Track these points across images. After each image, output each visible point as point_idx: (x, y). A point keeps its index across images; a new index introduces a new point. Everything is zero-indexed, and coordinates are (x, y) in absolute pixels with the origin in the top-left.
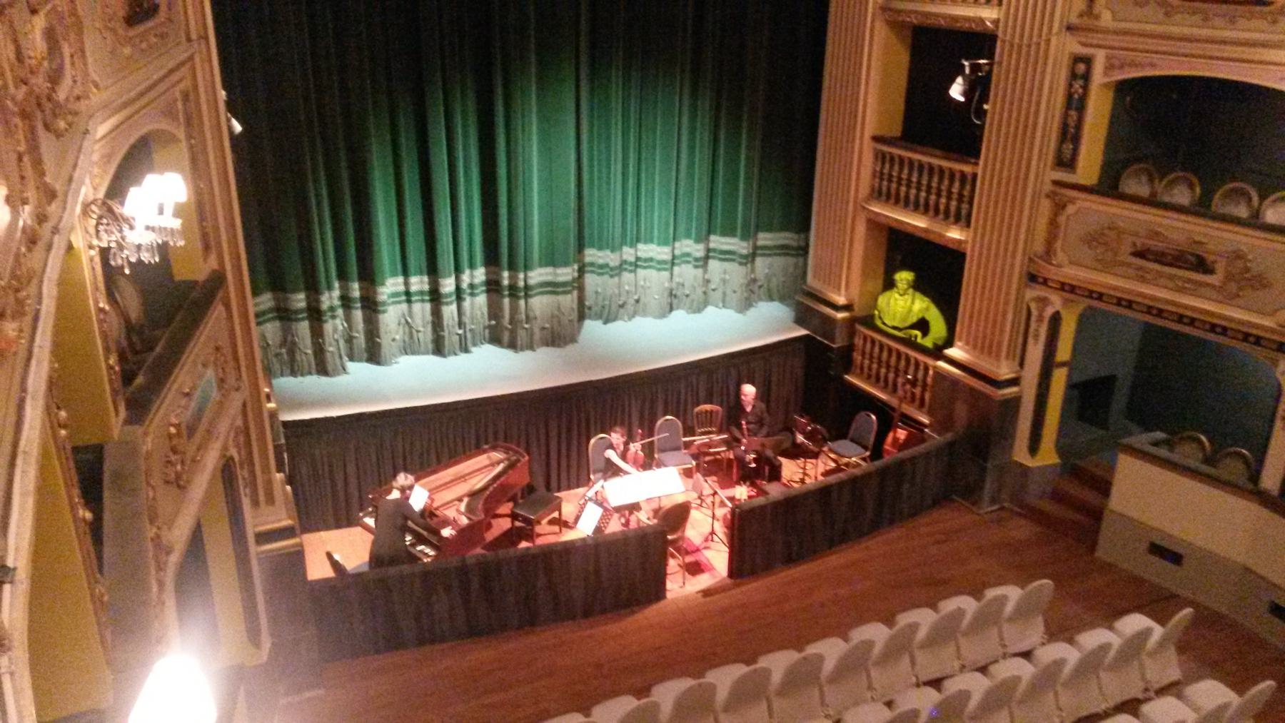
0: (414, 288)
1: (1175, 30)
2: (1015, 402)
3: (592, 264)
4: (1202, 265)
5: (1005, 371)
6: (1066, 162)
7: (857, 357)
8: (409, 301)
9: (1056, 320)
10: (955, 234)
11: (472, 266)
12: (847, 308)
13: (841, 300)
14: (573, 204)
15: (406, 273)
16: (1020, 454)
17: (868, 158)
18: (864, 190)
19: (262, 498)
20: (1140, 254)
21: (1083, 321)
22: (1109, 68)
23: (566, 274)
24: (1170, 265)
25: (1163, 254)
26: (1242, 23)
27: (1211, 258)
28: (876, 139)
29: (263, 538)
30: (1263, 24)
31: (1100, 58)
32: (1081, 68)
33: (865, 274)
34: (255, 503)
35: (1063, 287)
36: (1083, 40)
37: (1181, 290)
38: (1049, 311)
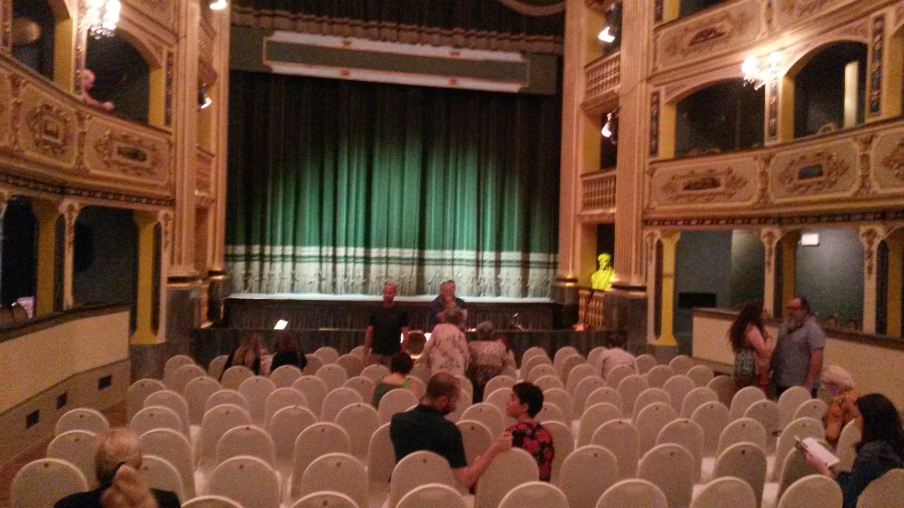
0: (324, 254)
1: (689, 62)
2: (644, 302)
3: (430, 260)
4: (715, 183)
5: (635, 281)
6: (654, 151)
7: (582, 313)
8: (321, 262)
9: (660, 246)
10: (612, 210)
11: (355, 246)
12: (574, 280)
13: (570, 276)
14: (405, 197)
15: (321, 244)
16: (651, 339)
17: (580, 185)
18: (580, 205)
19: (176, 260)
20: (687, 188)
21: (680, 249)
22: (667, 94)
23: (409, 253)
24: (700, 188)
25: (697, 184)
26: (716, 47)
27: (717, 177)
28: (583, 176)
29: (172, 280)
30: (723, 45)
31: (663, 90)
32: (655, 98)
33: (583, 259)
34: (172, 262)
35: (662, 222)
36: (656, 82)
37: (708, 201)
38: (656, 241)
